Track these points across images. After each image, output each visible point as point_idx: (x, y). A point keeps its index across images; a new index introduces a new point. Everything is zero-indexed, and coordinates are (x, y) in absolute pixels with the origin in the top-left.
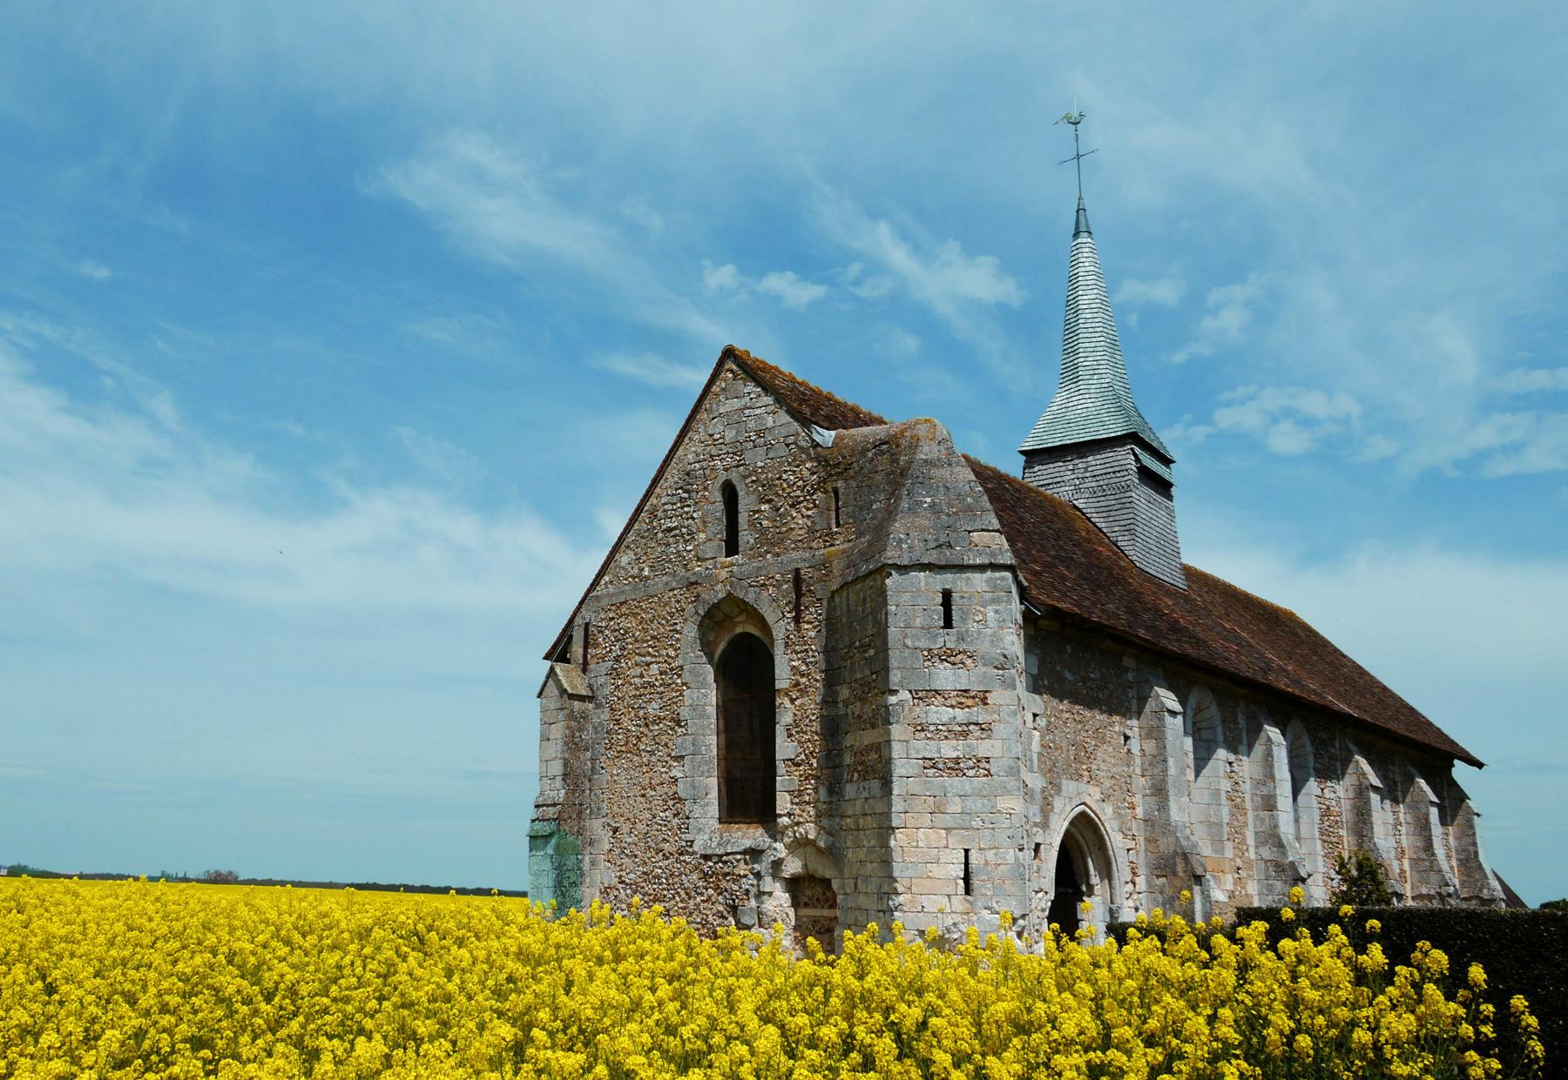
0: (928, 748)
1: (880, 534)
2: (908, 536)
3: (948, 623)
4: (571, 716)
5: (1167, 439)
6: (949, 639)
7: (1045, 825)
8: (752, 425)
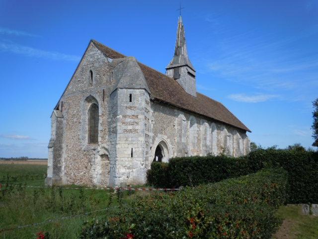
0: (124, 127)
1: (118, 81)
2: (124, 81)
3: (131, 101)
4: (57, 121)
5: (194, 66)
6: (130, 104)
7: (153, 143)
8: (96, 57)
